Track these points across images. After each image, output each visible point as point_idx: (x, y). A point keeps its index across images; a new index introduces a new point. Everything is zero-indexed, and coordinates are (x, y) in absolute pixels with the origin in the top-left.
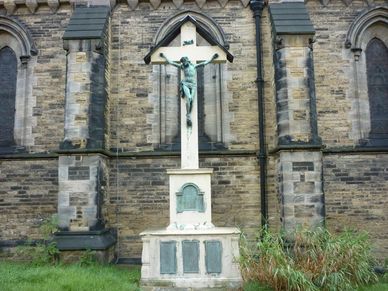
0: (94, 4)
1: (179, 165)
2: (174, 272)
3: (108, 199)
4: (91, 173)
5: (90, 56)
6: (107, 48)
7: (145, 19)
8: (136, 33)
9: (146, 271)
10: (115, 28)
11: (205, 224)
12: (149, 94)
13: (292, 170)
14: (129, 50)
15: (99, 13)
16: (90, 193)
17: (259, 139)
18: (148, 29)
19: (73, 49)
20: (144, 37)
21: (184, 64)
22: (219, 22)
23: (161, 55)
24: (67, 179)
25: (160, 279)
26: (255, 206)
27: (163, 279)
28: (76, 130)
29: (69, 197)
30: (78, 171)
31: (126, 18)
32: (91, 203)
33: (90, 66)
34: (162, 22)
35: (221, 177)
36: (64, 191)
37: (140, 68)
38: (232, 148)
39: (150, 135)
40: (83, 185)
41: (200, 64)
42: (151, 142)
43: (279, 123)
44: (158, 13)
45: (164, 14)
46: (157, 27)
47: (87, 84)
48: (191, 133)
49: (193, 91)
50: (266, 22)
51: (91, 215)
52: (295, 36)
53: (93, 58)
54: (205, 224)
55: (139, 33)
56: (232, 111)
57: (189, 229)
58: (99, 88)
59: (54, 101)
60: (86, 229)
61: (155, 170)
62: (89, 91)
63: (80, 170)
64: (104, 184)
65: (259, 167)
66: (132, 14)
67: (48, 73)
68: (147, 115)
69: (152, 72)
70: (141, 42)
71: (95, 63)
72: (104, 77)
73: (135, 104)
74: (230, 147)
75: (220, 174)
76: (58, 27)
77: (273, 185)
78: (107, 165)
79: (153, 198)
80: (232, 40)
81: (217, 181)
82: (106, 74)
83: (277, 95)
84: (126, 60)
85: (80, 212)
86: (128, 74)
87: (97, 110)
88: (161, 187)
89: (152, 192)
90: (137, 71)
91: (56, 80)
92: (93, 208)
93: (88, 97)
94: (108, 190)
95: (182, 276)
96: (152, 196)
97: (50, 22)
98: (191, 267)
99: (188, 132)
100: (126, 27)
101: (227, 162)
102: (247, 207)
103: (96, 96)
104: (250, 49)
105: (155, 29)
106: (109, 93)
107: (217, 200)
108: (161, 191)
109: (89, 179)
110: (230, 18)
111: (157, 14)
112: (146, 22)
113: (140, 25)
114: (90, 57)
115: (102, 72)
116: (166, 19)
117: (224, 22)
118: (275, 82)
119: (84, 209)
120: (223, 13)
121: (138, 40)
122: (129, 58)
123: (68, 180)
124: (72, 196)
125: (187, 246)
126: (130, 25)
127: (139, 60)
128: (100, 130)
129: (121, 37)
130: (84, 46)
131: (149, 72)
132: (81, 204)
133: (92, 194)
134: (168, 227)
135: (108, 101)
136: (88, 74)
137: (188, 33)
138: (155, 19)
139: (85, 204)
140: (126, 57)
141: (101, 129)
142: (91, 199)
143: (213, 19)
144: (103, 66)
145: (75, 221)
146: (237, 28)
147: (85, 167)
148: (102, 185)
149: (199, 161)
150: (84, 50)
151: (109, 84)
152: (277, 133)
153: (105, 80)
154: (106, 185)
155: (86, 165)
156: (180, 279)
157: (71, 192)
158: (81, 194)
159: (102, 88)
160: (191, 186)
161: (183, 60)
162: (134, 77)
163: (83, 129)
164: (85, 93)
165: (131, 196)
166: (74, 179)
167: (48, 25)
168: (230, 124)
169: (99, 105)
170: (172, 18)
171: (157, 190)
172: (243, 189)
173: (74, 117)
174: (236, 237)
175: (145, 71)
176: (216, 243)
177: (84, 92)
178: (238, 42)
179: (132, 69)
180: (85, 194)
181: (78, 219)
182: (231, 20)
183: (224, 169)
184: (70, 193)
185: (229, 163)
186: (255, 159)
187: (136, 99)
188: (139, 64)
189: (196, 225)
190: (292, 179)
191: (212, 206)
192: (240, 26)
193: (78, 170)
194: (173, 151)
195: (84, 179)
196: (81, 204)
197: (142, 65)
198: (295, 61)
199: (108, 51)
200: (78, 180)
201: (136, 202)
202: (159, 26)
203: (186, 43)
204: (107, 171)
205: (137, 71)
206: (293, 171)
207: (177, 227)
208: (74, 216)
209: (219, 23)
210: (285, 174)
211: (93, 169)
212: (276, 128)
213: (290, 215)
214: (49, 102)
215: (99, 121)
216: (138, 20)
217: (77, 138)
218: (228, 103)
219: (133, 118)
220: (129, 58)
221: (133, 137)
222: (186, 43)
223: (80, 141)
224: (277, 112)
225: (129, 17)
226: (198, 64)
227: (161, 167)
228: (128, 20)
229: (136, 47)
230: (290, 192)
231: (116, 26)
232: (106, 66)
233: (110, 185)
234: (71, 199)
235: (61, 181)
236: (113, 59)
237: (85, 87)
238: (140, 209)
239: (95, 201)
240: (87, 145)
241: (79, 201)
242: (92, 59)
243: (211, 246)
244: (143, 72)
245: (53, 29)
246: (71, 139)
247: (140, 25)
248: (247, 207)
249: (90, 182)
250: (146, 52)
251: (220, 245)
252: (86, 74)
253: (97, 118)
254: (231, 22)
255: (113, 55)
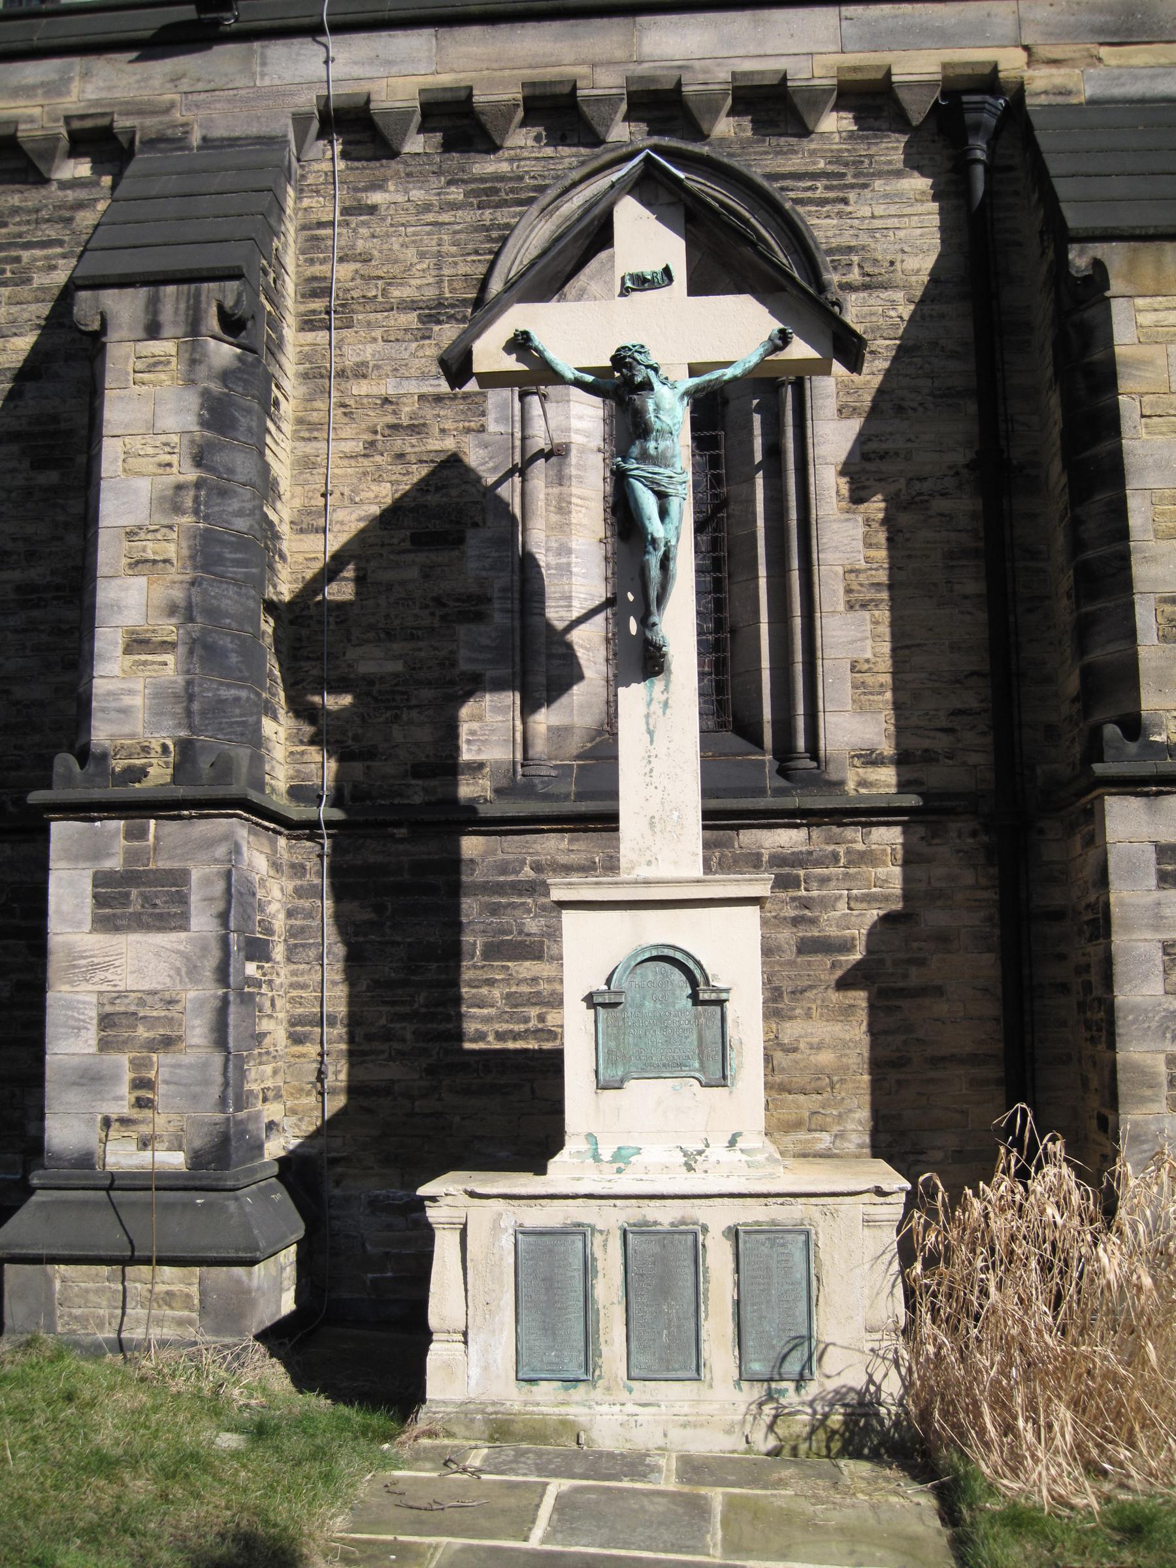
0: (219, 132)
1: (612, 865)
2: (586, 1372)
3: (279, 1022)
4: (194, 898)
5: (197, 356)
6: (275, 324)
7: (453, 189)
8: (411, 254)
9: (448, 1366)
10: (316, 238)
11: (732, 1143)
12: (470, 533)
13: (1153, 881)
14: (378, 333)
15: (239, 169)
16: (192, 994)
17: (989, 739)
18: (463, 236)
19: (120, 327)
20: (446, 272)
21: (621, 385)
22: (792, 195)
23: (520, 344)
24: (88, 926)
25: (517, 1407)
26: (973, 1059)
27: (530, 1408)
28: (127, 701)
29: (93, 1014)
30: (134, 892)
31: (366, 189)
32: (195, 1041)
33: (193, 400)
34: (530, 201)
35: (813, 921)
36: (71, 983)
37: (429, 412)
38: (862, 783)
39: (475, 726)
40: (157, 954)
41: (706, 377)
42: (482, 757)
43: (1089, 658)
44: (511, 160)
45: (538, 168)
46: (507, 226)
47: (179, 487)
48: (666, 704)
49: (674, 504)
50: (1016, 193)
51: (195, 1098)
52: (1153, 246)
53: (210, 368)
54: (732, 1143)
55: (422, 255)
56: (864, 606)
57: (654, 1167)
58: (235, 505)
59: (36, 574)
60: (177, 1160)
61: (499, 889)
62: (187, 520)
63: (149, 884)
64: (258, 950)
65: (994, 871)
66: (389, 173)
67: (15, 448)
68: (462, 630)
69: (482, 429)
70: (430, 293)
71: (215, 387)
72: (262, 454)
73: (402, 583)
74: (851, 778)
75: (805, 904)
76: (60, 243)
77: (1062, 957)
78: (276, 866)
79: (487, 1020)
80: (855, 276)
81: (786, 936)
82: (269, 440)
83: (1076, 523)
84: (364, 376)
85: (148, 1084)
86: (372, 444)
87: (226, 604)
88: (526, 969)
89: (484, 991)
90: (416, 429)
91: (52, 477)
92: (205, 1066)
93: (184, 544)
94: (278, 981)
95: (624, 1395)
96: (485, 1011)
97: (28, 222)
98: (670, 1354)
99: (649, 704)
100: (363, 231)
101: (841, 850)
102: (936, 1061)
103: (223, 543)
104: (942, 316)
105: (495, 234)
106: (284, 529)
107: (791, 1031)
108: (525, 989)
109: (185, 928)
110: (844, 175)
111: (505, 167)
112: (454, 206)
113: (430, 217)
114: (193, 362)
115: (250, 430)
116: (546, 187)
117: (818, 194)
118: (1067, 464)
119: (162, 1065)
120: (813, 153)
121: (419, 288)
122: (377, 367)
123: (94, 930)
124: (109, 1009)
125: (650, 1247)
126: (383, 219)
127: (423, 376)
128: (237, 699)
129: (343, 272)
130: (167, 313)
131: (468, 431)
132: (153, 1046)
133: (199, 994)
134: (557, 1158)
135: (279, 566)
136: (186, 439)
137: (645, 239)
138: (496, 191)
139: (168, 1043)
140: (364, 364)
141: (243, 694)
142: (197, 1022)
143: (766, 184)
144: (255, 405)
145: (124, 1121)
146: (878, 223)
147: (170, 872)
148: (250, 958)
149: (707, 845)
150: (167, 331)
151: (284, 486)
152: (1078, 706)
153: (266, 467)
154: (268, 959)
155: (176, 865)
156: (621, 1413)
157: (104, 988)
158: (149, 999)
159: (249, 505)
160: (669, 958)
161: (621, 360)
162: (400, 456)
163: (159, 694)
164: (171, 527)
165: (385, 1009)
166: (117, 929)
167: (20, 235)
168: (853, 668)
169: (236, 582)
170: (575, 185)
171: (507, 981)
172: (915, 976)
173: (120, 640)
174: (885, 1209)
175: (448, 425)
176: (789, 1237)
177: (166, 522)
178: (884, 287)
179: (391, 419)
180: (167, 996)
181: (135, 1114)
182: (852, 186)
183: (824, 881)
184: (100, 993)
185: (848, 852)
186: (974, 834)
187: (410, 557)
188: (422, 397)
189: (692, 1147)
190: (1156, 928)
191: (768, 1059)
192: (893, 210)
193: (138, 886)
194: (580, 796)
195: (160, 929)
196: (153, 1046)
197: (438, 399)
198: (1161, 362)
199: (281, 338)
200: (135, 931)
201: (409, 1036)
202: (513, 221)
203: (641, 283)
204: (276, 893)
205: (416, 429)
206: (1159, 887)
207: (596, 1157)
208: (121, 1103)
209: (796, 201)
210: (1122, 904)
211: (207, 881)
212: (1072, 684)
213: (1143, 1100)
214: (16, 575)
215: (234, 659)
216: (417, 195)
217: (132, 736)
218: (840, 570)
219: (396, 647)
220: (377, 367)
221: (397, 734)
222: (641, 283)
223: (146, 750)
224: (1078, 607)
225: (378, 185)
226: (696, 381)
227: (527, 873)
228: (376, 198)
229: (410, 319)
230: (1146, 990)
231: (321, 225)
232: (268, 406)
233: (289, 960)
234: (106, 1021)
235: (60, 938)
236: (305, 376)
237: (172, 501)
238: (430, 1071)
239: (212, 1030)
240: (177, 767)
241: (142, 1032)
242: (202, 371)
243: (765, 1250)
244: (443, 431)
245: (38, 253)
246: (107, 743)
247: (430, 217)
248: (936, 1061)
249: (190, 941)
250: (448, 333)
251: (807, 1243)
252: (175, 439)
253: (226, 642)
254: (852, 196)
255: (305, 358)
